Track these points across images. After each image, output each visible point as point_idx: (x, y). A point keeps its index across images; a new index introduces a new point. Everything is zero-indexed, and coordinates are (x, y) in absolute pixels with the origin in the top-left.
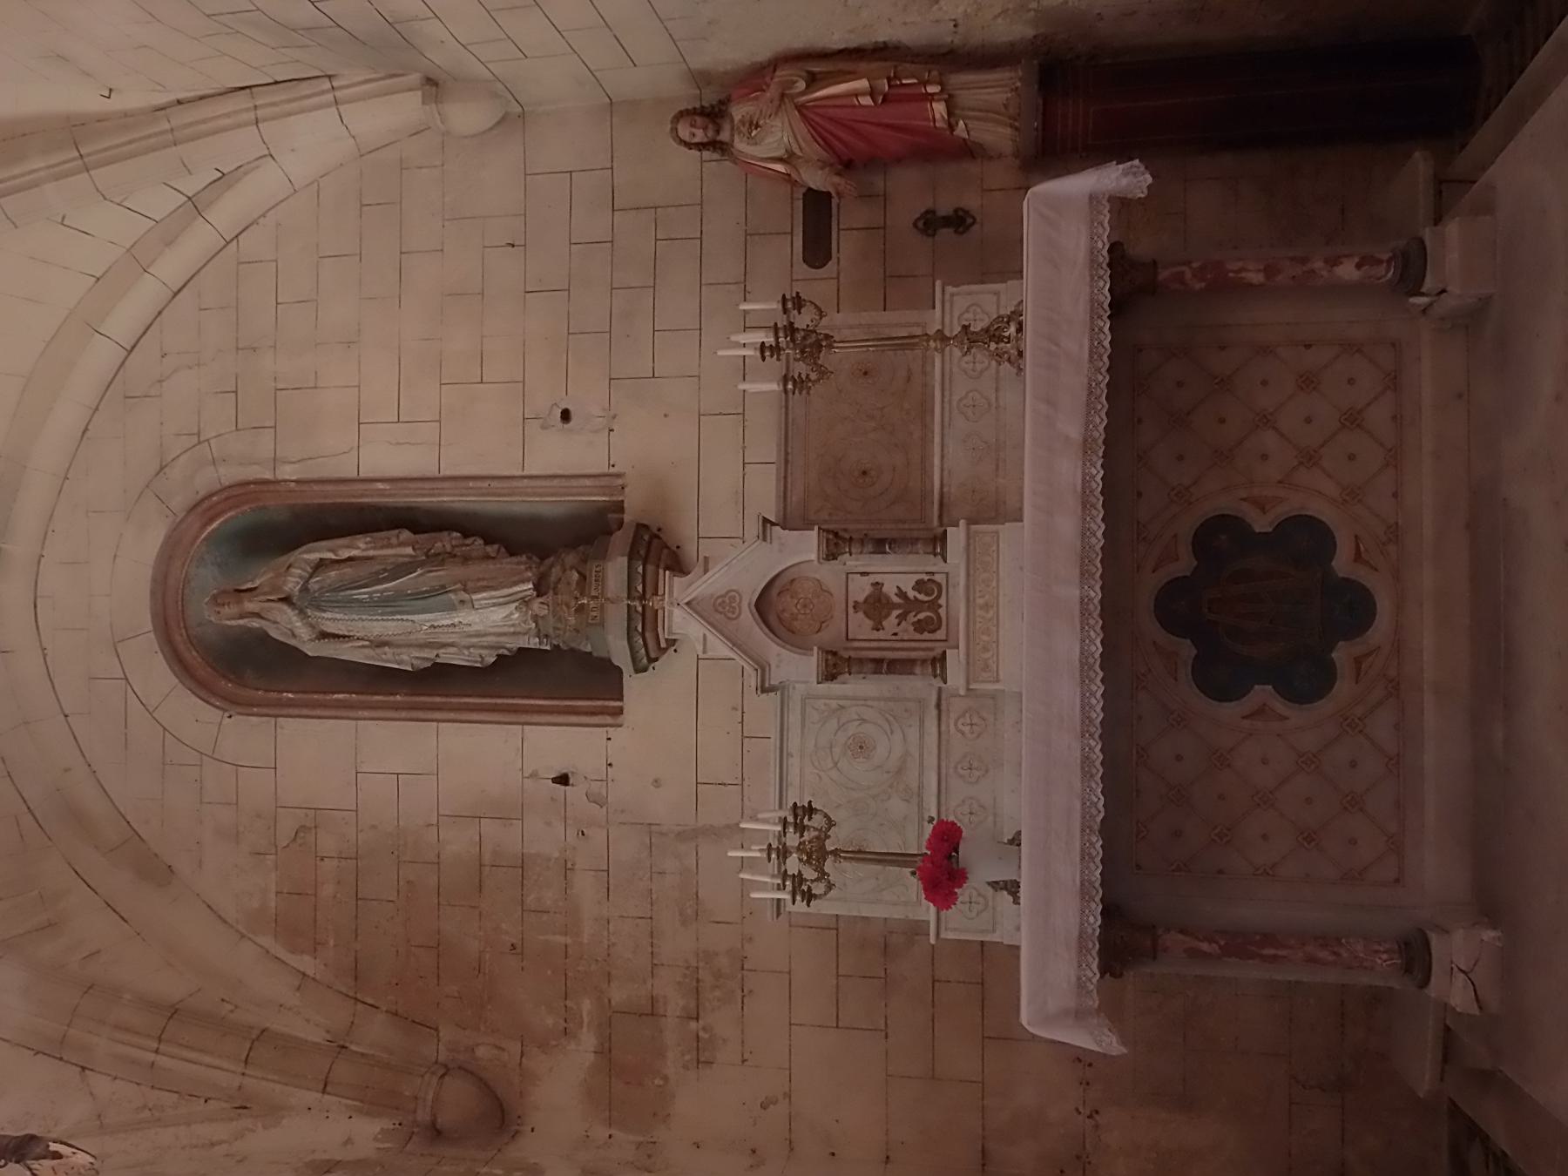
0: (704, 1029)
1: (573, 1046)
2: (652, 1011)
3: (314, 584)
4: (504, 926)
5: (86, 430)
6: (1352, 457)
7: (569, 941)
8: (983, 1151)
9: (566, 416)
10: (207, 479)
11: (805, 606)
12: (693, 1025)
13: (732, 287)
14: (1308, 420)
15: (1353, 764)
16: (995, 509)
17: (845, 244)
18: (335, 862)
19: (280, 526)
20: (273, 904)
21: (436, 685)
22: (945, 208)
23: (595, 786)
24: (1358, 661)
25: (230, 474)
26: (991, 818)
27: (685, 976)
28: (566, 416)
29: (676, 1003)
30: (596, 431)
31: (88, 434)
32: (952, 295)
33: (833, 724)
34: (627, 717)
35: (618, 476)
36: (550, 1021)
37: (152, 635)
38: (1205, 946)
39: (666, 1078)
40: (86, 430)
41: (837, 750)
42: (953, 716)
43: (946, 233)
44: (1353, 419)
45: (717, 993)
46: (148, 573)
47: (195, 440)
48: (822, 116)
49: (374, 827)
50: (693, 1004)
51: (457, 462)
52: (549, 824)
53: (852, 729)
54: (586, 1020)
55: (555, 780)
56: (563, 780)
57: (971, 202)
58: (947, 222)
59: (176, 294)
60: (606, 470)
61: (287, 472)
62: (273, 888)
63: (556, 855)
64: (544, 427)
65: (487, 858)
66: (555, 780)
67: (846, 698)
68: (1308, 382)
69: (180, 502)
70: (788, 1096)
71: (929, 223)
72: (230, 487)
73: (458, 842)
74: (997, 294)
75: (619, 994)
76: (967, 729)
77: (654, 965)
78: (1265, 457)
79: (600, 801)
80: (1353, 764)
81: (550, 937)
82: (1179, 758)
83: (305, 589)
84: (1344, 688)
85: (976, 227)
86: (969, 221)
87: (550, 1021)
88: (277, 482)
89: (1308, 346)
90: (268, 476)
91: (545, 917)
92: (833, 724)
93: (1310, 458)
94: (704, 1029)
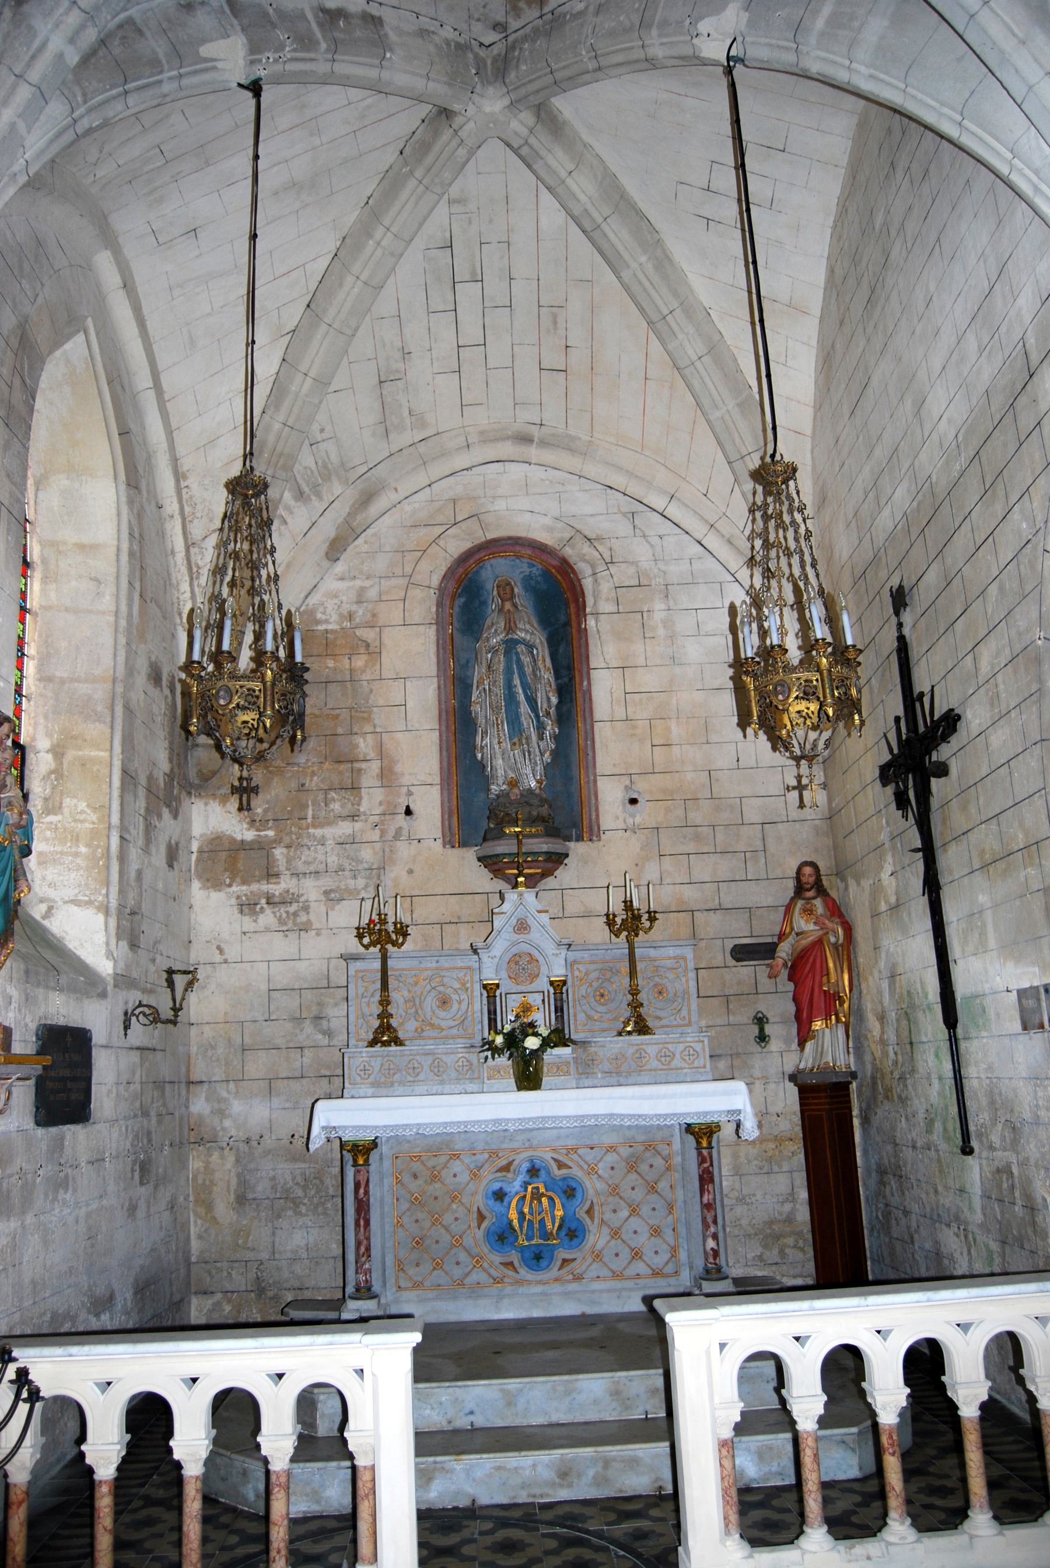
0: (262, 908)
1: (245, 826)
2: (271, 875)
3: (521, 648)
4: (315, 778)
5: (611, 488)
6: (617, 1255)
7: (309, 820)
8: (202, 1082)
9: (633, 801)
10: (583, 569)
11: (523, 969)
12: (264, 901)
13: (717, 901)
14: (635, 1232)
15: (458, 1263)
16: (11, 1382)
17: (746, 971)
18: (347, 667)
19: (557, 596)
20: (319, 628)
21: (459, 726)
22: (768, 1029)
23: (405, 832)
24: (511, 1264)
25: (588, 584)
26: (411, 1079)
27: (293, 894)
28: (633, 801)
29: (276, 889)
30: (625, 821)
31: (609, 490)
32: (703, 1041)
33: (457, 985)
34: (450, 851)
35: (599, 836)
36: (259, 811)
37: (484, 539)
38: (362, 1191)
39: (230, 885)
40: (611, 488)
41: (441, 989)
42: (467, 1055)
43: (755, 1030)
44: (637, 1254)
45: (284, 915)
46: (522, 533)
47: (608, 560)
48: (814, 961)
49: (371, 691)
50: (277, 900)
51: (603, 733)
52: (380, 804)
53: (455, 997)
54: (262, 833)
55: (408, 807)
56: (408, 812)
57: (775, 1045)
58: (762, 1030)
59: (699, 542)
60: (602, 828)
61: (591, 622)
62: (330, 627)
63: (362, 810)
64: (626, 787)
65: (356, 765)
66: (408, 807)
67: (472, 992)
68: (656, 1232)
69: (568, 552)
70: (226, 962)
71: (760, 1021)
72: (581, 586)
73: (365, 745)
74: (704, 1067)
75: (279, 853)
76: (460, 1063)
77: (298, 875)
78: (615, 1211)
79: (397, 836)
80: (458, 1263)
81: (310, 808)
82: (455, 1176)
83: (517, 642)
84: (497, 1258)
85: (760, 1049)
86: (763, 1045)
87: (259, 811)
88: (585, 615)
89: (674, 1230)
90: (588, 610)
91: (323, 804)
92: (457, 985)
93: (615, 1234)
94: (262, 908)
